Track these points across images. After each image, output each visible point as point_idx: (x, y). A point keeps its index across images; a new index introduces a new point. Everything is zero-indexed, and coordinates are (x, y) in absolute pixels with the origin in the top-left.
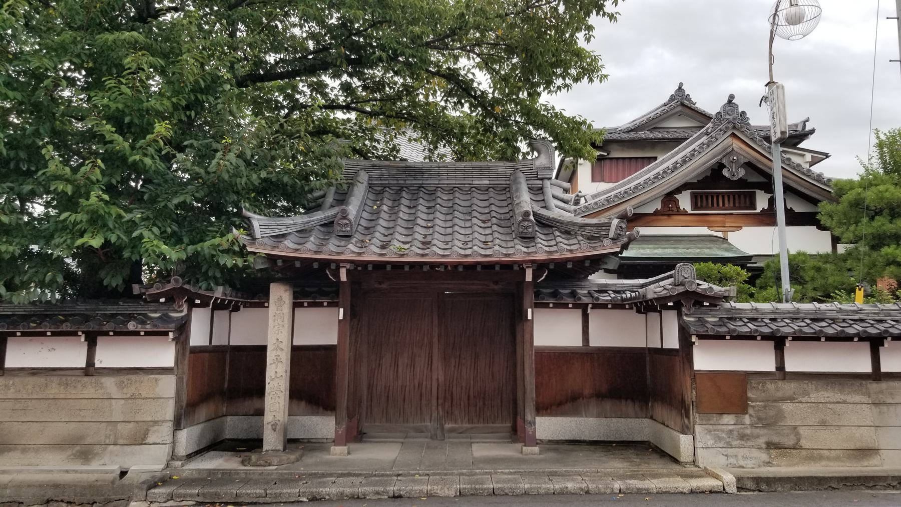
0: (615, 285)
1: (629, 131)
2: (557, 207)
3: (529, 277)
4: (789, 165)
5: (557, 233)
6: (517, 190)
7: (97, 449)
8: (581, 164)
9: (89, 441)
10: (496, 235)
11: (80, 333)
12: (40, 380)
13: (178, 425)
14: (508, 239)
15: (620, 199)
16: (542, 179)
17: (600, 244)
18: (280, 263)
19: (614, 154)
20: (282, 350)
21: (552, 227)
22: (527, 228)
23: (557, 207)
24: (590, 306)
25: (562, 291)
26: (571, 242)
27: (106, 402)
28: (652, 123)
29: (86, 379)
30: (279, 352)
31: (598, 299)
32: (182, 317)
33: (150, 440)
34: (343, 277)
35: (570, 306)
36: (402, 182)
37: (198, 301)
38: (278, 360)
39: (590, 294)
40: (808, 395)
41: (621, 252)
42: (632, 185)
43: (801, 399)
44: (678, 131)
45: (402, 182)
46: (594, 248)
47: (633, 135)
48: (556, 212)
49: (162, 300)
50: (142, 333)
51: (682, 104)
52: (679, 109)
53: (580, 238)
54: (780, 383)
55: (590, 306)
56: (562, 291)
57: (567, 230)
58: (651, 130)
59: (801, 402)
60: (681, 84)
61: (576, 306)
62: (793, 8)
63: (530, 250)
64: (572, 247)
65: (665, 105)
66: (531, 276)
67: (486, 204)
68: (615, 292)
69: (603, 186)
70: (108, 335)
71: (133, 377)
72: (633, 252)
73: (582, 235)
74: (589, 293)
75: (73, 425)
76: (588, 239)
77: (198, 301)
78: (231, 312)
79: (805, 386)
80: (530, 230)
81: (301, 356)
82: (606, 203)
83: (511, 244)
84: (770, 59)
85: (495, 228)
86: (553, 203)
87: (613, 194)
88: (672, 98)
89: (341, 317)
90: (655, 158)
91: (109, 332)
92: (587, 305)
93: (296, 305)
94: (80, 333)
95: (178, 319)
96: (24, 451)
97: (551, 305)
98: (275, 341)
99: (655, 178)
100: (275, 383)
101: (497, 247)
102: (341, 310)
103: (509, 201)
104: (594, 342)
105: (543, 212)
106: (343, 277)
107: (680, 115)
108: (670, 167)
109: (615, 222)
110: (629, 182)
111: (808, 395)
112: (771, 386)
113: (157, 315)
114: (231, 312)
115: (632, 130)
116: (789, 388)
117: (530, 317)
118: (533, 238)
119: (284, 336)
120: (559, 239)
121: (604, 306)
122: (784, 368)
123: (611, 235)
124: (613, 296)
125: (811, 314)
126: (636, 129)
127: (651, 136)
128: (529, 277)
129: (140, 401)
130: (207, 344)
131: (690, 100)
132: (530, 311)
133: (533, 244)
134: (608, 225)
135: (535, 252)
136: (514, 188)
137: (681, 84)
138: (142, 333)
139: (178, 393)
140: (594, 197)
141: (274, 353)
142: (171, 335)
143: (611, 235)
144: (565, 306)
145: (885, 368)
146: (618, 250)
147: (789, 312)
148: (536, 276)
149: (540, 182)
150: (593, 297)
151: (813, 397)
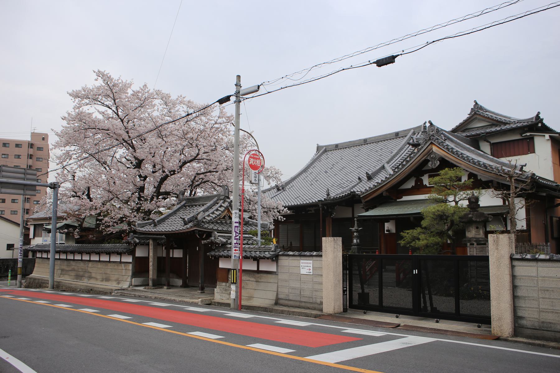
12: (114, 264)
81: (160, 261)
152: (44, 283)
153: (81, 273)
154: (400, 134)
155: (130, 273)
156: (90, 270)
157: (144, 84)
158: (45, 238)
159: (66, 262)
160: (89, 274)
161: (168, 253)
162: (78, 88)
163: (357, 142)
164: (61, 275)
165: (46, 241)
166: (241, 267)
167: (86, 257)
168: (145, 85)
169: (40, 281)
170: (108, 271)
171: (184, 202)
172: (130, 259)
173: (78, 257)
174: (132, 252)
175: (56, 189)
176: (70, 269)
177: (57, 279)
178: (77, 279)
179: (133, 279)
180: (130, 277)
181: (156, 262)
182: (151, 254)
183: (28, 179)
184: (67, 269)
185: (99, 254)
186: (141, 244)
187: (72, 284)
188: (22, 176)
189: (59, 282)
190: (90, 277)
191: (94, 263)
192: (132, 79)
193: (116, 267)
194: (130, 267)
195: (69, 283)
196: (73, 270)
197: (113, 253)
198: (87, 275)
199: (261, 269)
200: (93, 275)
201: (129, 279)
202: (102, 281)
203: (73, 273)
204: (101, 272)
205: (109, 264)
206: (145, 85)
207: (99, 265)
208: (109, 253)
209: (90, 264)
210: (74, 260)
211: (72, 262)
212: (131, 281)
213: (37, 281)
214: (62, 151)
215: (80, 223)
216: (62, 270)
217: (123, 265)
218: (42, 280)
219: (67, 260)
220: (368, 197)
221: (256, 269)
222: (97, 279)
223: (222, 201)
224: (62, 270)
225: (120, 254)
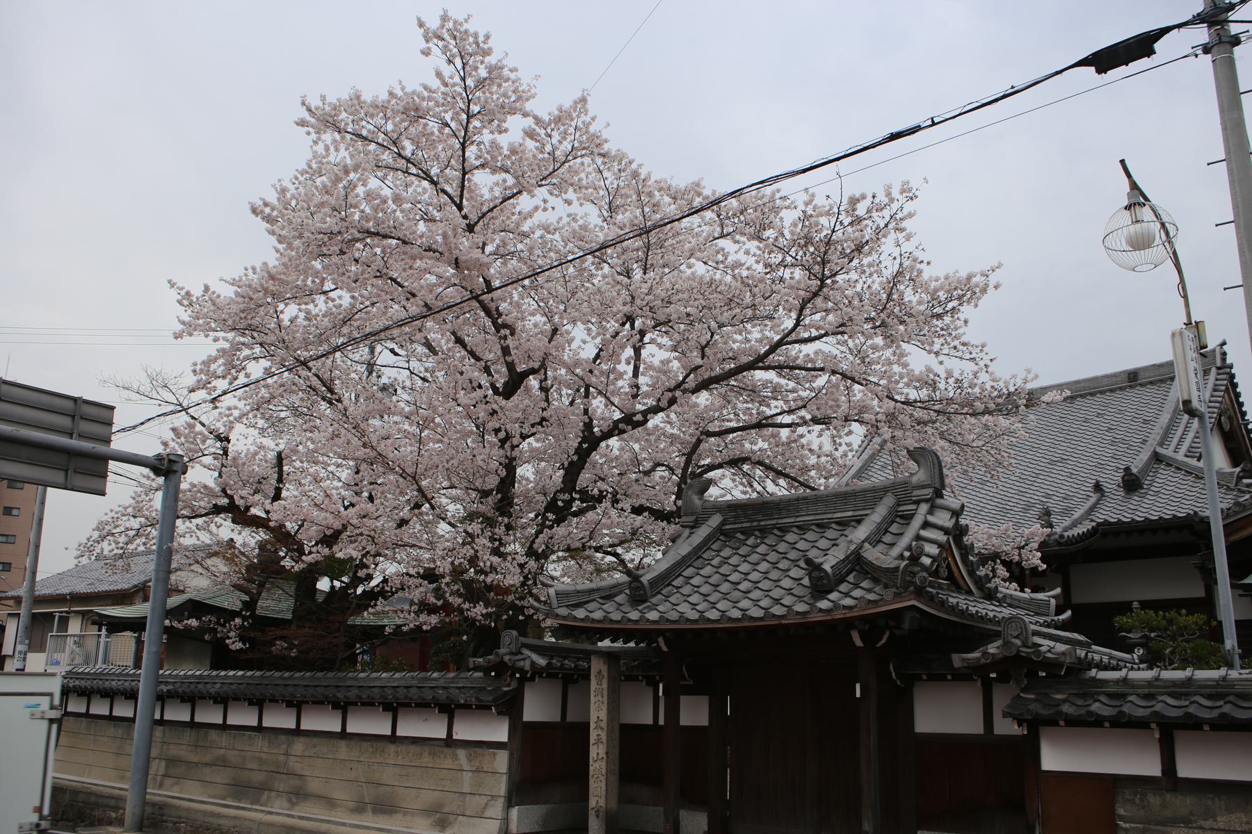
7: (451, 817)
9: (446, 810)
12: (414, 749)
13: (510, 803)
27: (459, 774)
29: (446, 750)
30: (600, 732)
33: (488, 814)
35: (924, 677)
38: (599, 741)
40: (1214, 817)
43: (1202, 823)
54: (1168, 796)
59: (1201, 828)
62: (1138, 226)
71: (479, 750)
75: (437, 793)
79: (1209, 802)
81: (630, 741)
84: (1184, 289)
94: (1153, 726)
96: (405, 814)
100: (597, 765)
104: (569, 719)
111: (1214, 817)
112: (1154, 800)
116: (1182, 803)
122: (1175, 771)
125: (1142, 687)
129: (482, 775)
130: (559, 720)
139: (510, 768)
145: (349, 730)
147: (1174, 683)
151: (1222, 821)
152: (97, 805)
153: (258, 777)
154: (1141, 375)
155: (502, 789)
156: (295, 765)
157: (578, 95)
158: (57, 656)
159: (188, 736)
160: (295, 782)
161: (673, 712)
162: (338, 93)
163: (1105, 382)
164: (168, 781)
165: (58, 663)
166: (162, 715)
167: (279, 719)
168: (583, 100)
169: (81, 797)
170: (389, 775)
171: (715, 520)
172: (500, 733)
173: (243, 717)
174: (510, 707)
175: (173, 477)
176: (207, 758)
177: (156, 793)
178: (237, 797)
179: (515, 812)
180: (499, 804)
181: (616, 743)
182: (598, 713)
183: (82, 436)
184: (194, 758)
185: (343, 707)
186: (547, 674)
187: (219, 816)
188: (65, 422)
189: (161, 807)
190: (299, 795)
191: (316, 740)
192: (538, 77)
193: (426, 759)
194: (501, 761)
195: (204, 813)
196: (222, 763)
197: (203, 697)
198: (282, 784)
199: (267, 723)
200: (313, 786)
201: (497, 809)
202: (359, 809)
203: (220, 776)
204: (352, 776)
205: (392, 748)
206: (583, 100)
207: (343, 750)
208: (394, 707)
209: (299, 746)
210: (224, 727)
211: (213, 735)
212: (506, 820)
213: (67, 796)
214: (216, 340)
215: (247, 598)
216: (172, 762)
217: (461, 753)
218: (91, 794)
219: (192, 724)
220: (1242, 528)
221: (221, 722)
222: (331, 803)
223: (924, 508)
224: (172, 762)
225: (449, 709)
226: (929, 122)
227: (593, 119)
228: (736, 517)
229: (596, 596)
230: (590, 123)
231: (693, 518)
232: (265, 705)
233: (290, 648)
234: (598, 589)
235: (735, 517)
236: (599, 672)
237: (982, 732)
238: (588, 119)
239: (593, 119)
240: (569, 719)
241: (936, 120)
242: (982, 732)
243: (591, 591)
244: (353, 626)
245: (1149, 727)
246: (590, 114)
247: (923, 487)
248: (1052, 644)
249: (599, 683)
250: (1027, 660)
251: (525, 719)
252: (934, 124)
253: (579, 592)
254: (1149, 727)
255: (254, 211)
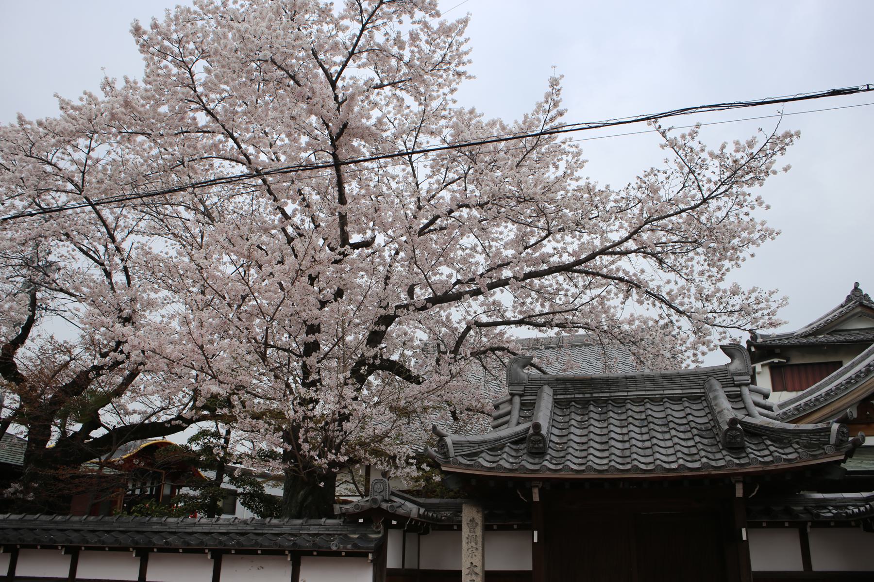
0: (835, 499)
1: (806, 335)
2: (761, 414)
3: (739, 492)
4: (789, 417)
5: (769, 442)
6: (715, 398)
8: (759, 373)
10: (700, 446)
11: (207, 551)
14: (714, 450)
15: (811, 407)
16: (739, 386)
17: (821, 451)
18: (474, 482)
19: (795, 361)
20: (477, 574)
21: (761, 436)
22: (736, 437)
23: (761, 414)
24: (809, 524)
25: (795, 508)
26: (787, 451)
28: (830, 326)
30: (474, 577)
31: (818, 515)
32: (380, 538)
34: (536, 498)
35: (787, 524)
36: (589, 395)
37: (394, 522)
39: (807, 511)
41: (844, 461)
42: (823, 391)
44: (862, 333)
45: (589, 395)
46: (815, 457)
47: (812, 339)
48: (759, 419)
49: (361, 521)
50: (343, 554)
51: (861, 305)
52: (859, 309)
53: (796, 446)
55: (809, 524)
56: (795, 508)
57: (779, 437)
58: (831, 334)
60: (857, 284)
61: (792, 525)
63: (743, 461)
64: (790, 457)
65: (842, 306)
66: (742, 491)
67: (682, 414)
68: (836, 507)
69: (786, 396)
70: (231, 553)
72: (851, 465)
73: (798, 443)
74: (805, 509)
76: (805, 447)
77: (394, 522)
78: (420, 534)
80: (739, 439)
82: (796, 412)
83: (719, 456)
85: (697, 439)
86: (756, 410)
87: (802, 402)
88: (849, 299)
89: (536, 540)
90: (840, 364)
91: (312, 551)
92: (805, 523)
93: (487, 528)
95: (376, 539)
97: (764, 524)
98: (469, 565)
99: (847, 383)
101: (704, 460)
102: (536, 533)
103: (707, 410)
104: (406, 567)
105: (748, 419)
106: (536, 498)
107: (860, 316)
108: (863, 370)
109: (835, 426)
110: (818, 389)
113: (356, 536)
114: (405, 532)
115: (810, 335)
117: (744, 538)
118: (742, 449)
119: (477, 561)
120: (772, 448)
121: (825, 524)
123: (833, 440)
124: (834, 511)
126: (815, 332)
127: (832, 339)
128: (739, 492)
131: (869, 300)
132: (744, 531)
133: (744, 455)
134: (828, 429)
135: (749, 464)
136: (711, 396)
137: (857, 284)
138: (343, 554)
140: (781, 406)
141: (469, 578)
142: (370, 556)
143: (833, 440)
144: (781, 525)
146: (842, 457)
148: (746, 491)
149: (738, 389)
150: (812, 514)
157: (463, 16)
168: (465, 22)
206: (465, 22)
226: (866, 88)
227: (466, 40)
228: (566, 389)
229: (484, 447)
230: (462, 43)
231: (522, 388)
232: (151, 555)
233: (26, 492)
234: (486, 442)
235: (565, 389)
236: (473, 520)
237: (802, 569)
238: (461, 39)
239: (466, 40)
240: (406, 567)
241: (871, 87)
242: (802, 569)
243: (480, 443)
244: (198, 473)
245: (204, 553)
246: (465, 35)
247: (741, 374)
248: (403, 502)
249: (472, 529)
250: (384, 512)
251: (388, 567)
252: (868, 89)
253: (470, 443)
254: (204, 553)
255: (137, 31)
